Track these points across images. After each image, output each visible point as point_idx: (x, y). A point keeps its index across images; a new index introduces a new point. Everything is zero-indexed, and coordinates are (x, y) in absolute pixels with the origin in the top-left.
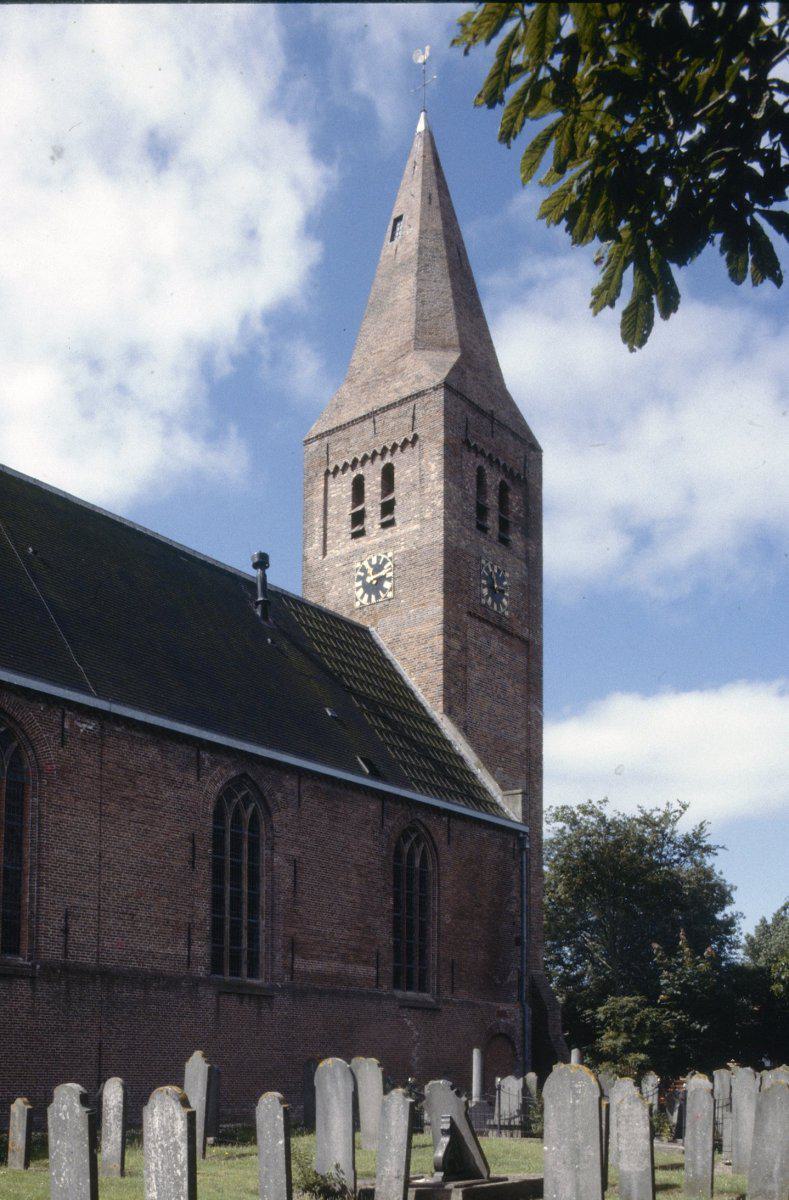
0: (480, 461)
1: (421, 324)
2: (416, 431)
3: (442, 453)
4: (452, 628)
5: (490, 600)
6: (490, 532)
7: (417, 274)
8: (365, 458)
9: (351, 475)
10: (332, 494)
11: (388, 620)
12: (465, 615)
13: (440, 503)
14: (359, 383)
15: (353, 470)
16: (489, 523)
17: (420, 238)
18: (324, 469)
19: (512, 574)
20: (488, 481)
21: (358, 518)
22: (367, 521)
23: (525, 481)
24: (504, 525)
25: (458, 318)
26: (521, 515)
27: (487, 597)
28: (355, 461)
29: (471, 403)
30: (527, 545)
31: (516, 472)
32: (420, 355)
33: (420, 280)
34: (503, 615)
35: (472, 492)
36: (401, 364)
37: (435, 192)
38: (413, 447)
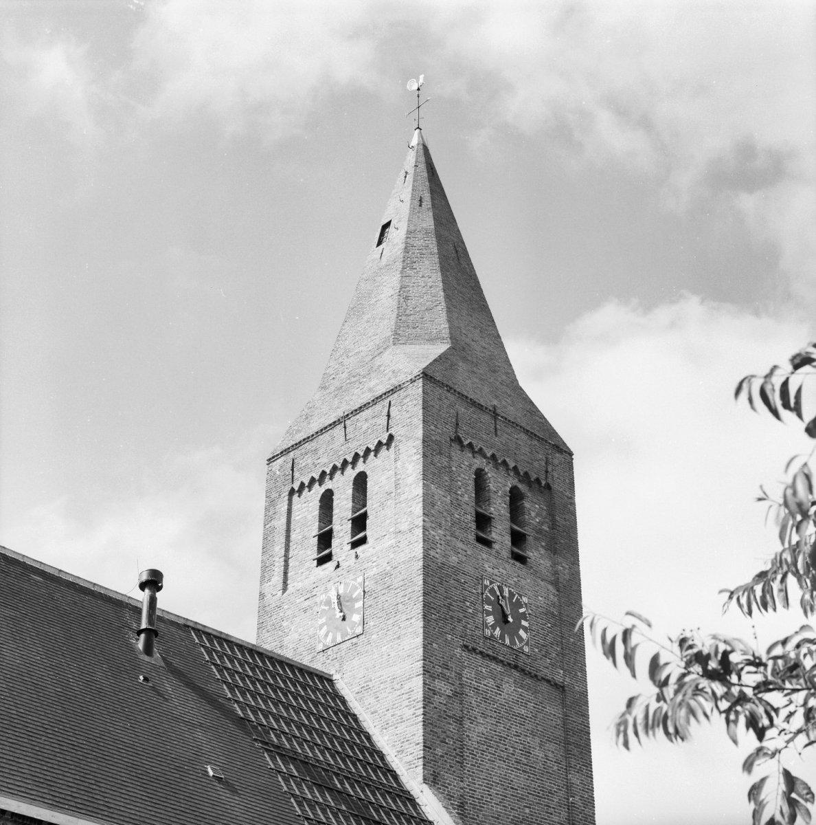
0: (479, 462)
1: (404, 318)
2: (392, 431)
3: (421, 451)
4: (434, 667)
5: (498, 632)
6: (496, 546)
7: (401, 273)
8: (335, 468)
9: (318, 490)
10: (296, 516)
11: (356, 662)
12: (459, 650)
13: (418, 509)
14: (332, 388)
15: (320, 485)
16: (494, 536)
17: (407, 238)
18: (288, 488)
19: (531, 593)
20: (492, 486)
21: (325, 539)
22: (335, 542)
23: (548, 487)
24: (518, 538)
25: (449, 310)
26: (545, 528)
27: (494, 627)
28: (323, 474)
29: (462, 397)
30: (554, 564)
31: (534, 477)
32: (399, 349)
33: (403, 275)
34: (521, 651)
35: (467, 496)
36: (378, 361)
37: (427, 197)
38: (388, 449)
